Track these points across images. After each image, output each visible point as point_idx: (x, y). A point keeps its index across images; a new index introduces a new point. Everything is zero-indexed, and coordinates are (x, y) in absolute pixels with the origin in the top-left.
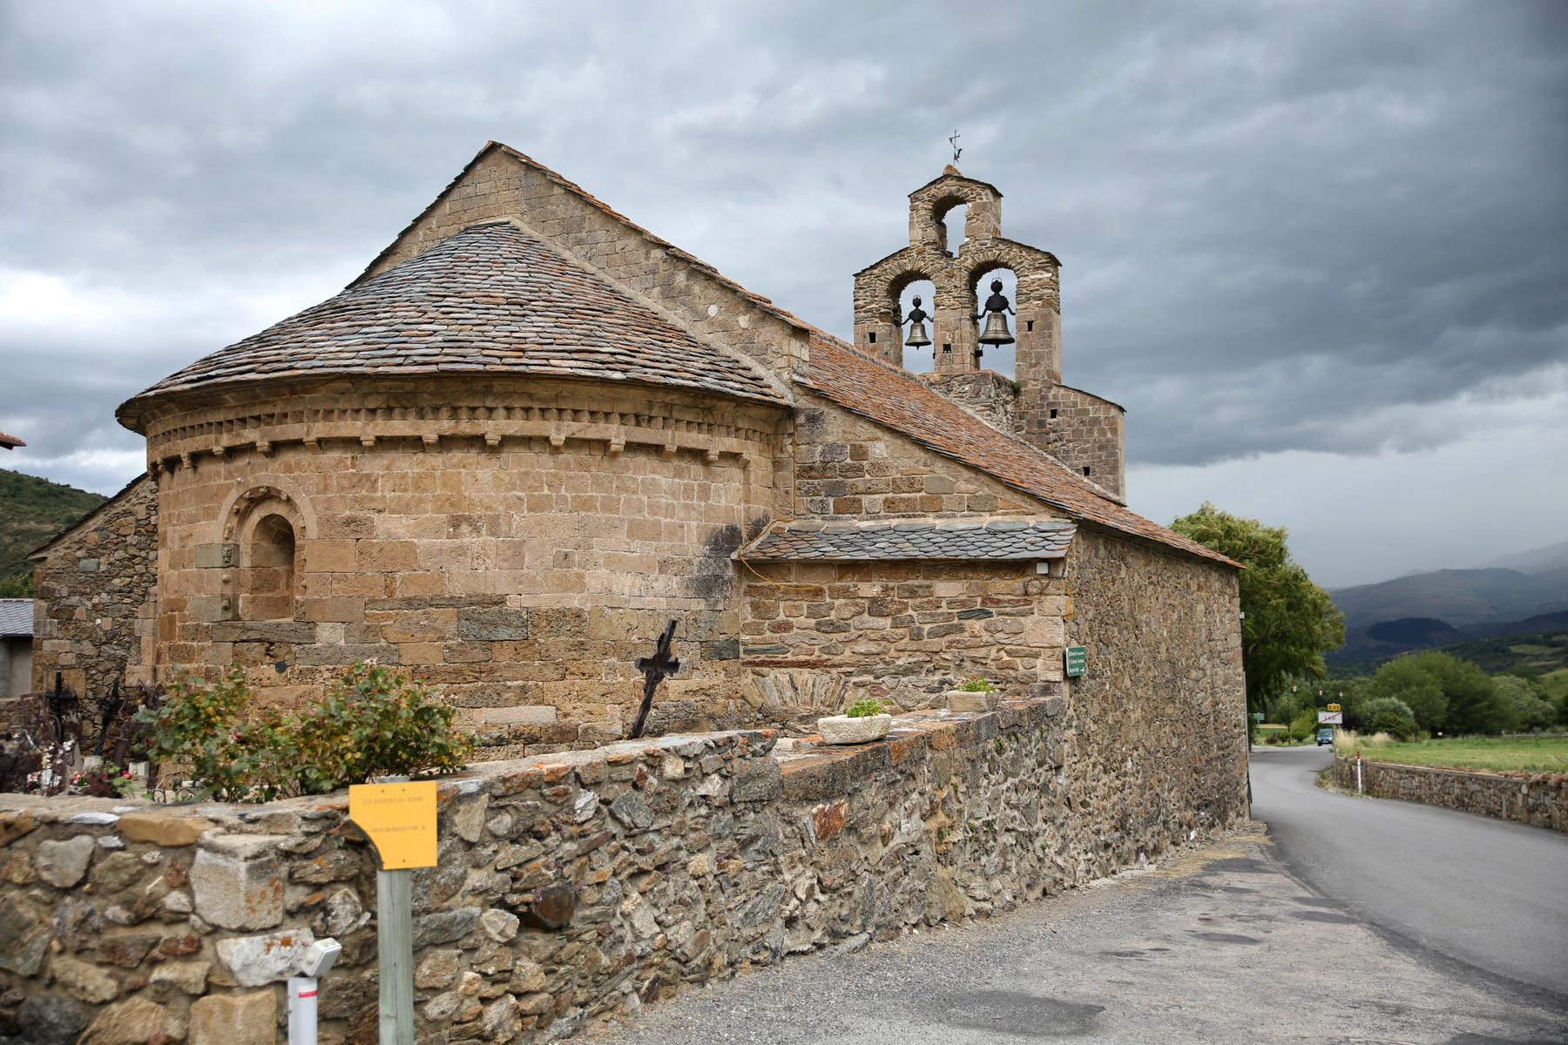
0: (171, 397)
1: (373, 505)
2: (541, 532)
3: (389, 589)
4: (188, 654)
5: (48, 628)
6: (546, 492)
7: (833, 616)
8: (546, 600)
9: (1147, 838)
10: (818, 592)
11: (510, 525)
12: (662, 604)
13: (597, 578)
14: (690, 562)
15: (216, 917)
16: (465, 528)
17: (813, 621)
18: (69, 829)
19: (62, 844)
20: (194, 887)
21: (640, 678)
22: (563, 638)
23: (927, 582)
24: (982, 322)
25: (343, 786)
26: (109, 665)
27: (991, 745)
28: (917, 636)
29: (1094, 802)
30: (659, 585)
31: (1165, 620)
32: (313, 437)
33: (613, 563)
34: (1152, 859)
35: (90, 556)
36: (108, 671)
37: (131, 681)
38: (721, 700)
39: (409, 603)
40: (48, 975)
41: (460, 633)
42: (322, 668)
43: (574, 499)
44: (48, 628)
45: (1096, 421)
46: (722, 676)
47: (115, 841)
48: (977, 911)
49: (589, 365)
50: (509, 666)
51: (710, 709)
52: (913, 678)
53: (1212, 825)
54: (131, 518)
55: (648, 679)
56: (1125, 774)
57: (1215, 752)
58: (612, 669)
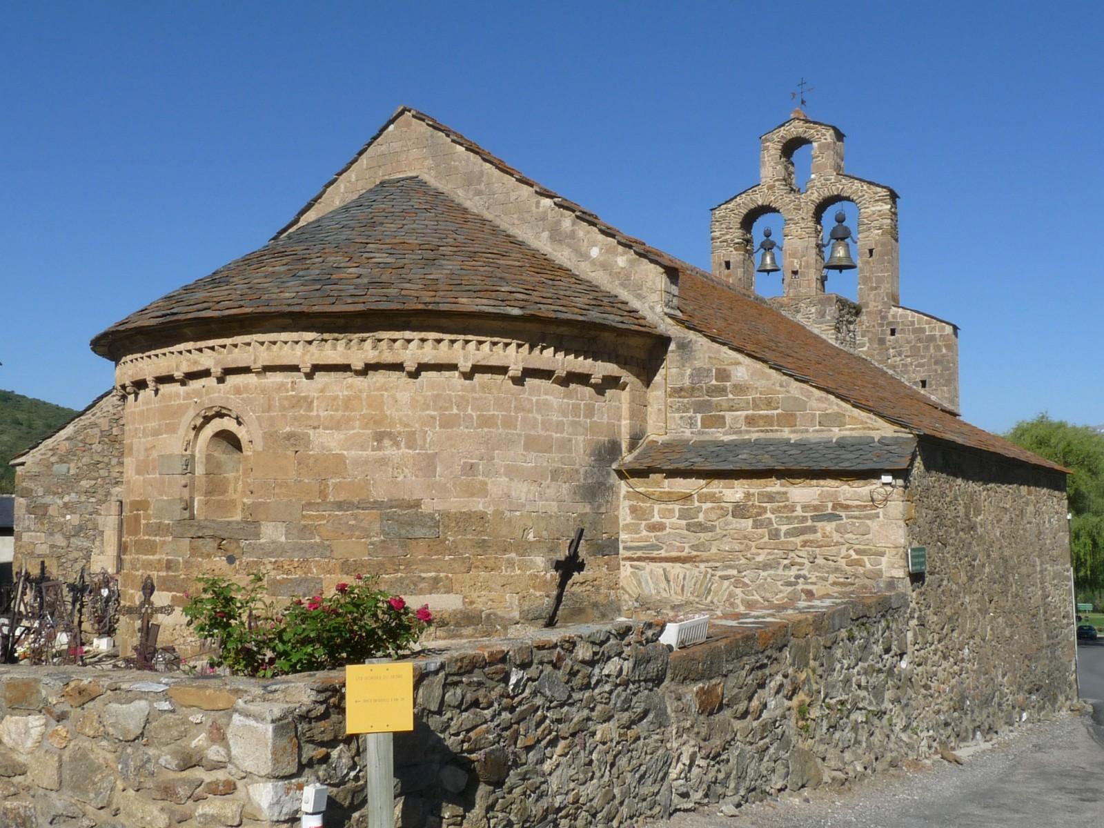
0: (140, 331)
1: (310, 422)
2: (452, 446)
3: (323, 494)
4: (151, 548)
5: (27, 523)
6: (455, 411)
7: (701, 518)
8: (455, 503)
9: (981, 717)
10: (687, 497)
11: (425, 440)
12: (553, 508)
13: (498, 485)
14: (577, 471)
15: (248, 764)
16: (387, 442)
17: (684, 522)
18: (130, 695)
19: (124, 706)
20: (231, 742)
21: (553, 575)
22: (469, 537)
23: (783, 489)
24: (827, 251)
25: (338, 664)
26: (76, 554)
27: (843, 633)
28: (775, 535)
29: (934, 685)
30: (551, 492)
31: (998, 521)
32: (260, 364)
33: (513, 472)
34: (988, 737)
35: (61, 461)
36: (76, 560)
37: (96, 567)
38: (603, 591)
39: (340, 505)
40: (114, 807)
41: (383, 532)
42: (266, 561)
43: (478, 417)
44: (27, 523)
45: (932, 338)
46: (604, 569)
47: (166, 706)
48: (833, 779)
49: (492, 302)
50: (423, 561)
51: (594, 598)
52: (772, 572)
53: (1042, 708)
54: (96, 430)
55: (561, 576)
56: (963, 660)
57: (1045, 642)
58: (511, 564)
